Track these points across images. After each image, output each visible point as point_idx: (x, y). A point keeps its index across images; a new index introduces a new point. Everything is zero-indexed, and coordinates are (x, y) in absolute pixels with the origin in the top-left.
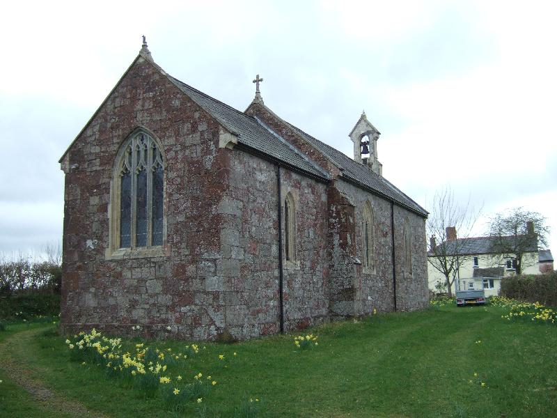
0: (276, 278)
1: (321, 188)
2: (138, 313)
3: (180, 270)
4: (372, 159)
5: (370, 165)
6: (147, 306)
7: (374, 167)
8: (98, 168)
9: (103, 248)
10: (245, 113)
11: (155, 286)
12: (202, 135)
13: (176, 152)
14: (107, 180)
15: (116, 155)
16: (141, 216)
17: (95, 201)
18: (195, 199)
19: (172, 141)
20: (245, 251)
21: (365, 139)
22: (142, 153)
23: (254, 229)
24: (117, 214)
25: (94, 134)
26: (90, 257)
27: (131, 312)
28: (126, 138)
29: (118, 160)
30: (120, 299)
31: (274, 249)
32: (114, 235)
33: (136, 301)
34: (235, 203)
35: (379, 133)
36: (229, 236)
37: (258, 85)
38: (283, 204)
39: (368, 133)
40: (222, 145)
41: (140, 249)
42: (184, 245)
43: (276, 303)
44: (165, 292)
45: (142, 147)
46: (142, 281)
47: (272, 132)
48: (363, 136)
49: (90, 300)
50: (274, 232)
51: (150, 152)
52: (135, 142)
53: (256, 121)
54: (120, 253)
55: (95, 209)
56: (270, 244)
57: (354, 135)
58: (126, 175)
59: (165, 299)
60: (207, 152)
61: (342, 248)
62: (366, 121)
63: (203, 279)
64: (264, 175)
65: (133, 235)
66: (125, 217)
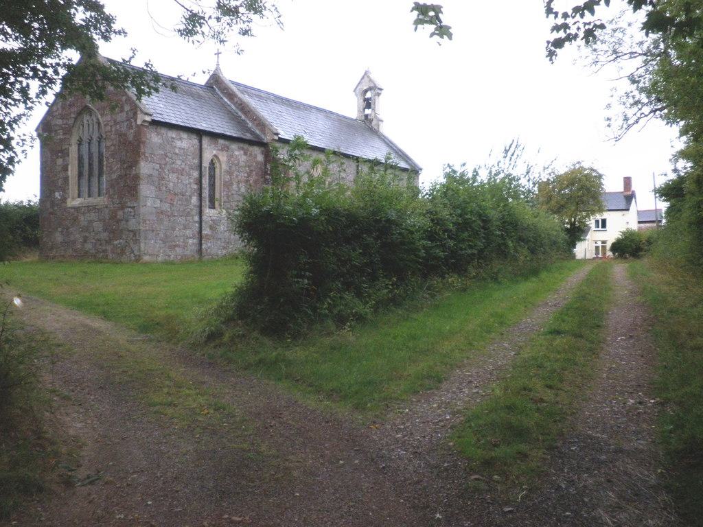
0: (196, 222)
1: (257, 152)
2: (88, 246)
3: (113, 216)
4: (373, 115)
5: (371, 121)
6: (94, 241)
7: (374, 123)
8: (62, 137)
9: (66, 199)
10: (205, 86)
11: (98, 226)
12: (127, 114)
13: (111, 126)
14: (67, 146)
15: (73, 126)
16: (91, 174)
17: (60, 161)
18: (123, 162)
19: (109, 118)
20: (161, 201)
21: (369, 95)
22: (91, 126)
23: (171, 184)
24: (76, 173)
25: (58, 109)
26: (58, 205)
27: (83, 245)
28: (80, 114)
29: (74, 130)
30: (77, 236)
31: (194, 200)
32: (73, 188)
33: (87, 237)
34: (151, 165)
35: (381, 89)
36: (146, 190)
37: (218, 57)
38: (206, 164)
39: (370, 89)
40: (139, 122)
41: (90, 199)
42: (116, 196)
43: (196, 241)
44: (105, 230)
45: (90, 122)
46: (90, 222)
47: (226, 100)
48: (366, 91)
49: (59, 237)
50: (195, 187)
51: (96, 126)
52: (86, 118)
53: (215, 90)
54: (77, 202)
55: (60, 168)
56: (190, 197)
57: (357, 91)
58: (80, 143)
59: (104, 235)
60: (130, 127)
61: (639, 247)
62: (368, 77)
63: (127, 221)
64: (186, 143)
65: (86, 189)
66: (80, 175)
